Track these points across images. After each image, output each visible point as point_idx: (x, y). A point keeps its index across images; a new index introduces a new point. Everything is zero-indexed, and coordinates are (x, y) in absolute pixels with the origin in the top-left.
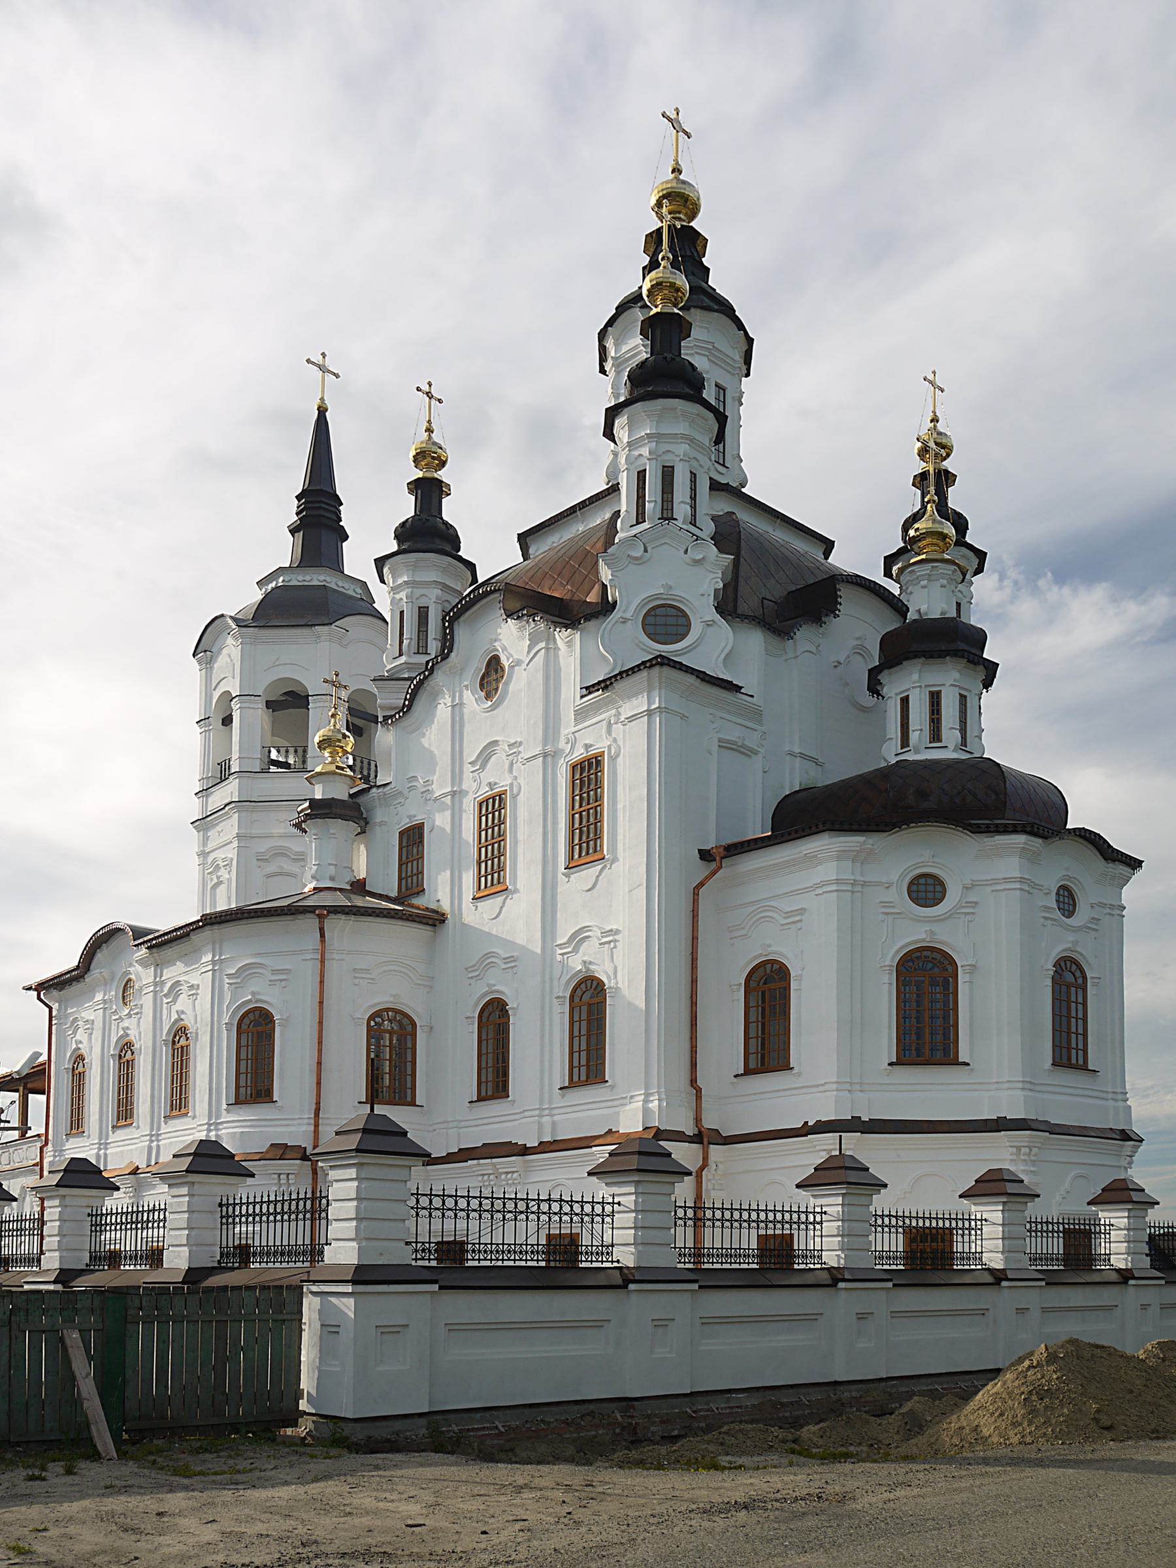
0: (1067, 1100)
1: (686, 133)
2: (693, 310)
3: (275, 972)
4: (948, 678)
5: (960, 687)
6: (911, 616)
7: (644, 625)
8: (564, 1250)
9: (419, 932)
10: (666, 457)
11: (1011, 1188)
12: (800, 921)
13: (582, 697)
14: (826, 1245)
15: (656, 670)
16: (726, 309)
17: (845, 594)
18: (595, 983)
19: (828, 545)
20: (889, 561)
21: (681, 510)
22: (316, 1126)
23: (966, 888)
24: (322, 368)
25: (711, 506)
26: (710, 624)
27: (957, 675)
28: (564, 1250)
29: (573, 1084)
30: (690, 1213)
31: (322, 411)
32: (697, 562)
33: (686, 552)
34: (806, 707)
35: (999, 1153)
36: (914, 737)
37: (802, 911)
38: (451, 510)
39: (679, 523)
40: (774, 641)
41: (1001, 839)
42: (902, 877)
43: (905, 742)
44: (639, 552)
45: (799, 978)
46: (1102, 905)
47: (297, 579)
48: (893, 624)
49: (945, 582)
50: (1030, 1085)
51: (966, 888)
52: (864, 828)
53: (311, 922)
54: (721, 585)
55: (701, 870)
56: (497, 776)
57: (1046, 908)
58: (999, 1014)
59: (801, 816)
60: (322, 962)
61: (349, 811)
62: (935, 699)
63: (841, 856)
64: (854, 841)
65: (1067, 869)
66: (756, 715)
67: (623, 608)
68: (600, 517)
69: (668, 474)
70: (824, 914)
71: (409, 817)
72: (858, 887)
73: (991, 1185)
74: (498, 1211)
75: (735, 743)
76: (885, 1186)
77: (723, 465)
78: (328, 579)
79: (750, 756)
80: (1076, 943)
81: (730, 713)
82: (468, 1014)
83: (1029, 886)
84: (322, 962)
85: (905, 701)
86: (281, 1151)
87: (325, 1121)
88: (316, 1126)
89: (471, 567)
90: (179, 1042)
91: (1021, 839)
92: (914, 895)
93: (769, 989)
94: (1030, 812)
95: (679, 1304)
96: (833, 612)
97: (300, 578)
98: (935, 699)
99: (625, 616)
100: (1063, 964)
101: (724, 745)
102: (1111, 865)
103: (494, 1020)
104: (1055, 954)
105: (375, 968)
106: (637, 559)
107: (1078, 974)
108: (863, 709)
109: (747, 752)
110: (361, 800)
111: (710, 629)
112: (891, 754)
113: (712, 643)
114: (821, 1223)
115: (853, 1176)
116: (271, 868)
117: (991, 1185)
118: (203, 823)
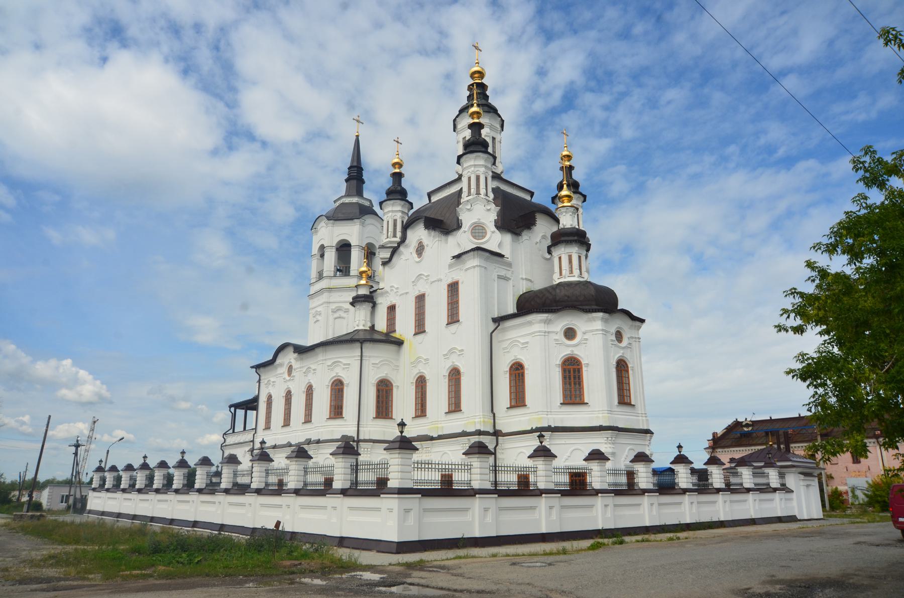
0: (623, 418)
3: (345, 364)
7: (472, 233)
8: (447, 480)
9: (393, 348)
14: (541, 481)
15: (476, 252)
19: (532, 194)
21: (483, 191)
25: (492, 184)
26: (493, 232)
28: (447, 480)
29: (450, 412)
31: (357, 136)
32: (489, 210)
35: (601, 442)
36: (564, 272)
37: (527, 343)
38: (405, 183)
40: (515, 237)
46: (632, 338)
48: (555, 229)
50: (610, 412)
53: (358, 345)
55: (492, 326)
56: (421, 288)
57: (612, 340)
58: (598, 381)
59: (529, 304)
61: (368, 299)
63: (541, 321)
64: (544, 316)
66: (509, 265)
68: (454, 189)
69: (478, 178)
70: (538, 344)
83: (605, 332)
85: (560, 258)
89: (411, 204)
90: (309, 391)
91: (601, 314)
93: (517, 371)
94: (602, 301)
95: (492, 502)
101: (500, 277)
103: (421, 383)
104: (616, 357)
105: (378, 363)
108: (549, 259)
109: (506, 279)
113: (495, 240)
116: (336, 315)
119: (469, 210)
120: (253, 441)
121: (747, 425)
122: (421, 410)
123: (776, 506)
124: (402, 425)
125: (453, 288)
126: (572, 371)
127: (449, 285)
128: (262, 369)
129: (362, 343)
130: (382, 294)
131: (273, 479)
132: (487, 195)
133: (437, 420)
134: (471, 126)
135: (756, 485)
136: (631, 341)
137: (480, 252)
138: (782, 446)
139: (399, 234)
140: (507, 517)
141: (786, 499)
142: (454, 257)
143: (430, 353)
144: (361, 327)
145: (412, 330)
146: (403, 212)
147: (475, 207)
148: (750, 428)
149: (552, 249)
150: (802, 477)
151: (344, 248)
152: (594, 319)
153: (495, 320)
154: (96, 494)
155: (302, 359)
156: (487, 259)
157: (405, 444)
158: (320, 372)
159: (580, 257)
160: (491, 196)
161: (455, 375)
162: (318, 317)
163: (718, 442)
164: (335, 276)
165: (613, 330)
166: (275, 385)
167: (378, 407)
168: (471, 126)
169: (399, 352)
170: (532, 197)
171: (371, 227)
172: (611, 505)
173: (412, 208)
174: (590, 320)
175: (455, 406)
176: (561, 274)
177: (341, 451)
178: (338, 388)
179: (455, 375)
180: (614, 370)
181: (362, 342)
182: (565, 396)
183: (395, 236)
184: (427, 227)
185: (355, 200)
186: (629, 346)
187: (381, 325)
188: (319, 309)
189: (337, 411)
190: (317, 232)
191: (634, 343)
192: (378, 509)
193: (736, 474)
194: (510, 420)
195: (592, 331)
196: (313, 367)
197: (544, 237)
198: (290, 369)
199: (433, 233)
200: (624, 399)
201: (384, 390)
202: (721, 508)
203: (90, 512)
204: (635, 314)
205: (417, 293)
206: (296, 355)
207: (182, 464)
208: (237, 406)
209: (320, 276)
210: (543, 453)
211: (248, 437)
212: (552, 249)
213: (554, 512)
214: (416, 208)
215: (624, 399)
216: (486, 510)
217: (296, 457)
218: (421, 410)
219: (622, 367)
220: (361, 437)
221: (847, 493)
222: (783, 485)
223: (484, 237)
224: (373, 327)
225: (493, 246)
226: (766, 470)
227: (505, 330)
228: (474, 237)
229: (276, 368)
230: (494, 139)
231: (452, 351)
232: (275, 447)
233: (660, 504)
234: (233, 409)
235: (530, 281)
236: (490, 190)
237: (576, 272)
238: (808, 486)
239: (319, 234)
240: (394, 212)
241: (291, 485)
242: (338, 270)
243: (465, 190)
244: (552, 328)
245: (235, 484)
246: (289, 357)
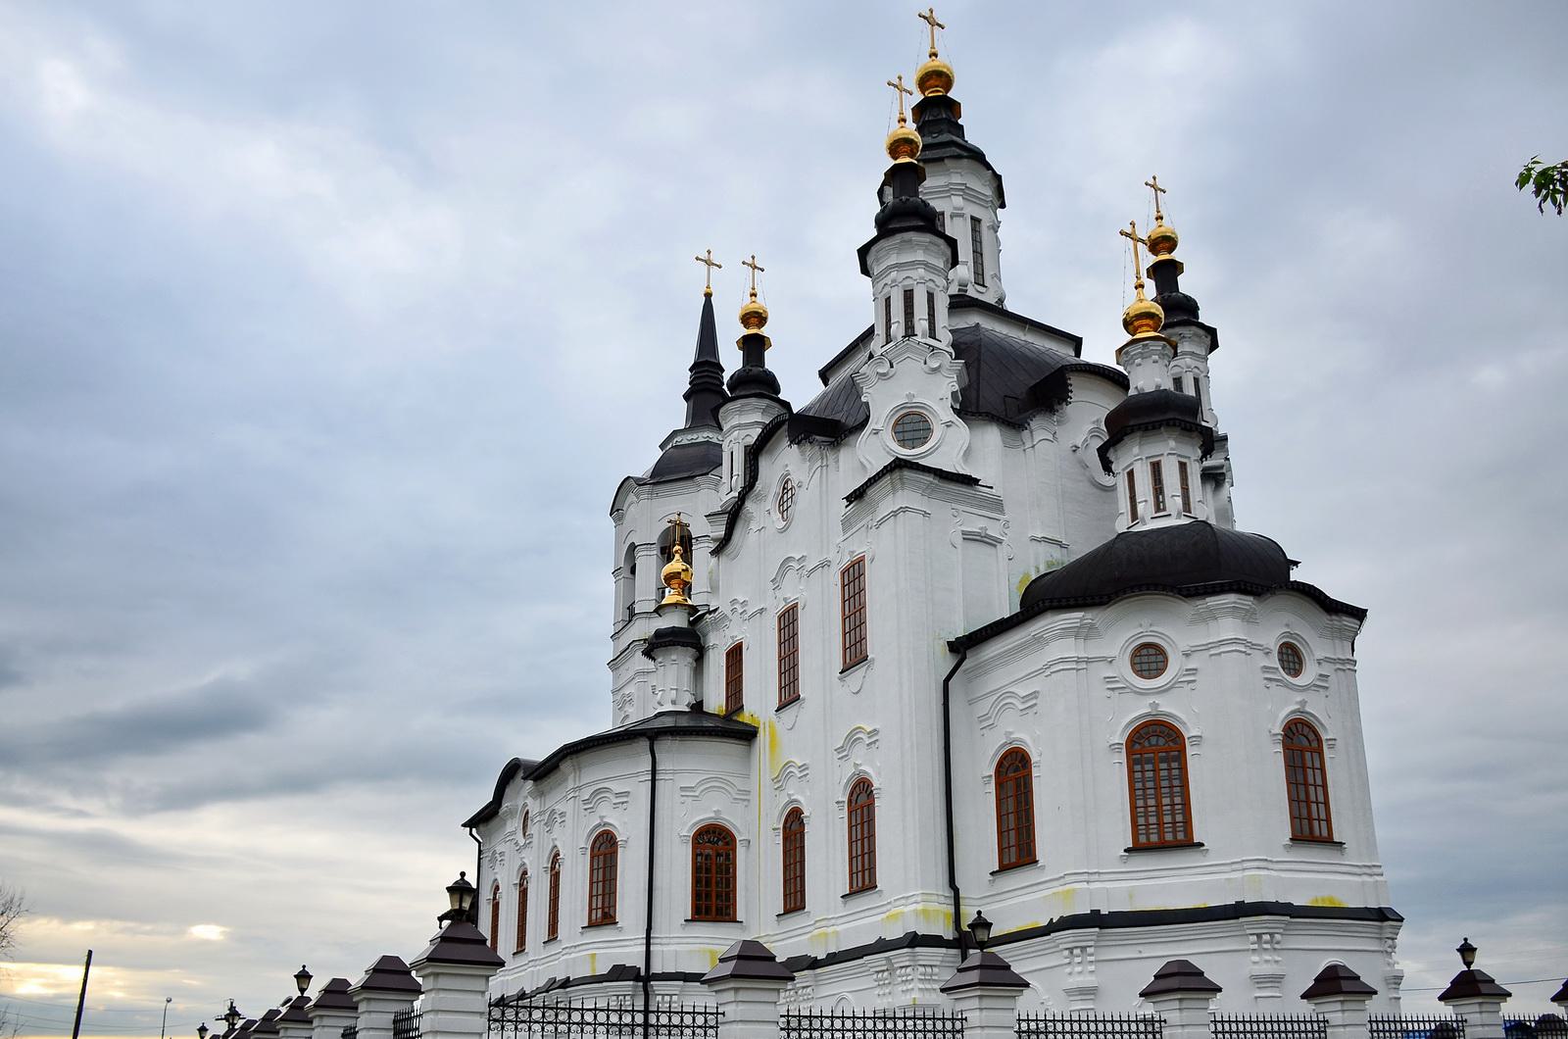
0: (1308, 880)
1: (940, 25)
2: (946, 161)
5: (1179, 456)
10: (906, 282)
11: (1345, 985)
12: (1035, 704)
13: (847, 507)
15: (896, 474)
16: (977, 156)
17: (1075, 381)
18: (609, 836)
20: (1119, 351)
21: (921, 325)
22: (648, 945)
24: (709, 263)
26: (949, 424)
27: (1172, 443)
30: (639, 1018)
31: (708, 296)
32: (935, 370)
33: (925, 363)
34: (1044, 493)
37: (1035, 695)
38: (772, 361)
39: (918, 339)
40: (1010, 433)
42: (1124, 649)
43: (1134, 515)
47: (684, 440)
49: (1157, 357)
52: (1097, 600)
53: (644, 744)
54: (957, 388)
56: (793, 590)
57: (1266, 669)
60: (654, 781)
61: (687, 639)
65: (1287, 625)
66: (997, 505)
67: (875, 420)
69: (909, 296)
70: (1070, 699)
71: (732, 637)
74: (688, 1027)
75: (979, 534)
76: (1220, 990)
77: (983, 286)
78: (711, 435)
79: (995, 546)
80: (1303, 703)
81: (972, 506)
82: (775, 826)
84: (654, 781)
85: (1131, 474)
87: (639, 942)
88: (648, 945)
91: (1231, 598)
92: (1138, 667)
93: (1014, 773)
94: (1255, 572)
96: (1065, 400)
97: (690, 437)
98: (1156, 468)
99: (876, 427)
100: (1294, 729)
101: (969, 537)
102: (1334, 617)
105: (697, 787)
106: (884, 375)
107: (1312, 736)
109: (992, 542)
111: (951, 428)
112: (1122, 525)
113: (952, 444)
114: (961, 1031)
115: (1193, 982)
118: (614, 664)
122: (794, 900)
125: (853, 577)
126: (1156, 750)
132: (933, 335)
133: (831, 920)
136: (1326, 669)
143: (806, 753)
149: (1111, 455)
152: (1213, 615)
156: (928, 492)
159: (1183, 466)
161: (861, 799)
167: (697, 895)
169: (748, 756)
175: (863, 878)
178: (605, 848)
179: (861, 799)
184: (795, 440)
186: (1321, 685)
187: (716, 701)
194: (1014, 905)
195: (1207, 647)
196: (560, 808)
200: (1311, 828)
201: (714, 852)
204: (1334, 593)
215: (1311, 828)
218: (794, 900)
219: (1302, 744)
220: (656, 969)
223: (924, 440)
227: (982, 669)
230: (975, 221)
231: (852, 739)
244: (1094, 649)
246: (522, 794)
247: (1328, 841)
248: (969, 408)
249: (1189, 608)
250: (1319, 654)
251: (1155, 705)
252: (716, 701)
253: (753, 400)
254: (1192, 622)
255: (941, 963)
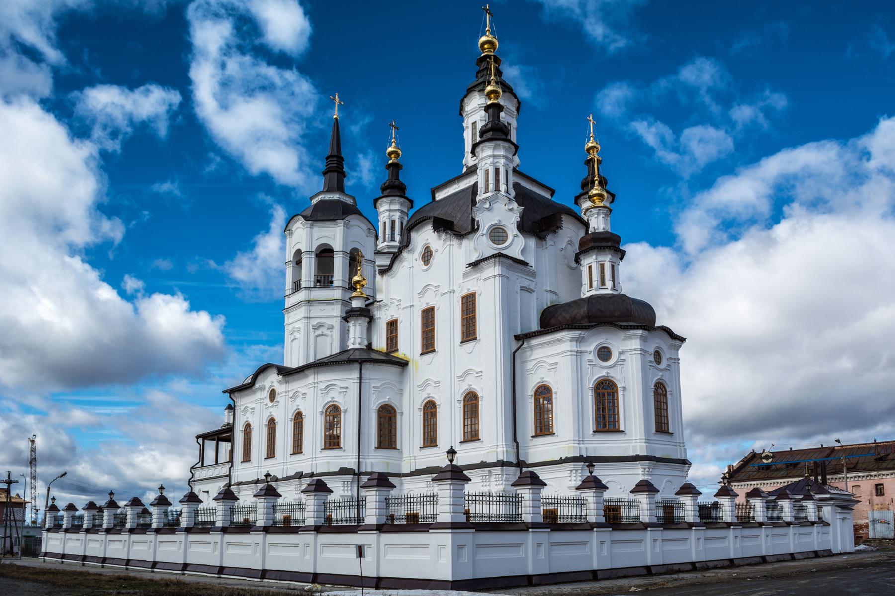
0: (662, 449)
3: (341, 388)
4: (607, 259)
6: (591, 231)
7: (491, 236)
9: (395, 369)
21: (503, 187)
22: (359, 459)
23: (620, 353)
25: (512, 179)
26: (516, 236)
29: (425, 447)
32: (511, 210)
40: (539, 241)
41: (632, 332)
44: (487, 206)
45: (556, 393)
46: (671, 358)
50: (648, 440)
51: (620, 353)
53: (357, 365)
55: (515, 345)
56: (429, 300)
57: (651, 361)
58: (633, 408)
59: (553, 321)
60: (361, 383)
62: (602, 267)
63: (572, 339)
66: (533, 274)
70: (557, 362)
72: (579, 353)
73: (645, 487)
83: (644, 352)
85: (590, 267)
86: (343, 471)
89: (411, 201)
90: (298, 419)
91: (640, 332)
93: (544, 393)
95: (545, 536)
101: (523, 289)
103: (430, 409)
105: (380, 384)
108: (572, 269)
109: (529, 290)
110: (370, 308)
113: (517, 245)
116: (319, 332)
117: (645, 487)
119: (488, 209)
120: (229, 476)
121: (767, 457)
123: (814, 540)
124: (452, 452)
126: (606, 394)
127: (463, 298)
128: (236, 394)
129: (361, 363)
130: (379, 308)
131: (279, 516)
134: (487, 108)
135: (769, 518)
137: (502, 259)
138: (820, 478)
139: (398, 238)
140: (621, 550)
141: (823, 533)
142: (470, 265)
144: (357, 346)
145: (419, 349)
146: (402, 211)
147: (495, 206)
148: (770, 460)
150: (839, 510)
151: (325, 254)
152: (631, 337)
153: (517, 338)
154: (51, 535)
155: (287, 382)
156: (509, 268)
157: (456, 474)
158: (310, 396)
160: (513, 193)
162: (297, 335)
163: (733, 475)
164: (315, 287)
165: (652, 350)
166: (253, 411)
168: (487, 108)
169: (402, 374)
170: (552, 195)
171: (356, 229)
172: (660, 540)
173: (412, 207)
174: (625, 339)
176: (591, 286)
177: (313, 488)
178: (333, 413)
180: (653, 394)
181: (361, 362)
182: (598, 423)
183: (393, 239)
184: (436, 229)
185: (336, 196)
187: (380, 343)
188: (297, 325)
189: (332, 442)
190: (291, 234)
191: (673, 365)
192: (426, 546)
193: (776, 508)
197: (570, 243)
198: (273, 395)
199: (443, 236)
202: (764, 543)
203: (46, 554)
205: (424, 307)
206: (281, 377)
207: (162, 501)
208: (205, 437)
209: (297, 287)
210: (594, 484)
211: (224, 470)
212: (582, 257)
213: (543, 550)
214: (417, 206)
216: (539, 545)
217: (223, 499)
218: (472, 435)
220: (363, 470)
221: (867, 526)
222: (820, 518)
223: (504, 241)
224: (370, 346)
225: (515, 252)
226: (805, 503)
227: (531, 348)
228: (494, 241)
229: (254, 392)
231: (467, 373)
232: (239, 484)
233: (742, 537)
234: (200, 440)
235: (555, 293)
236: (511, 186)
237: (609, 283)
238: (844, 519)
239: (295, 236)
240: (389, 211)
241: (219, 524)
242: (318, 281)
243: (481, 185)
245: (197, 524)
246: (272, 380)
247: (667, 432)
248: (523, 227)
249: (622, 334)
250: (668, 356)
251: (608, 373)
252: (380, 343)
253: (397, 198)
254: (623, 340)
255: (513, 473)
